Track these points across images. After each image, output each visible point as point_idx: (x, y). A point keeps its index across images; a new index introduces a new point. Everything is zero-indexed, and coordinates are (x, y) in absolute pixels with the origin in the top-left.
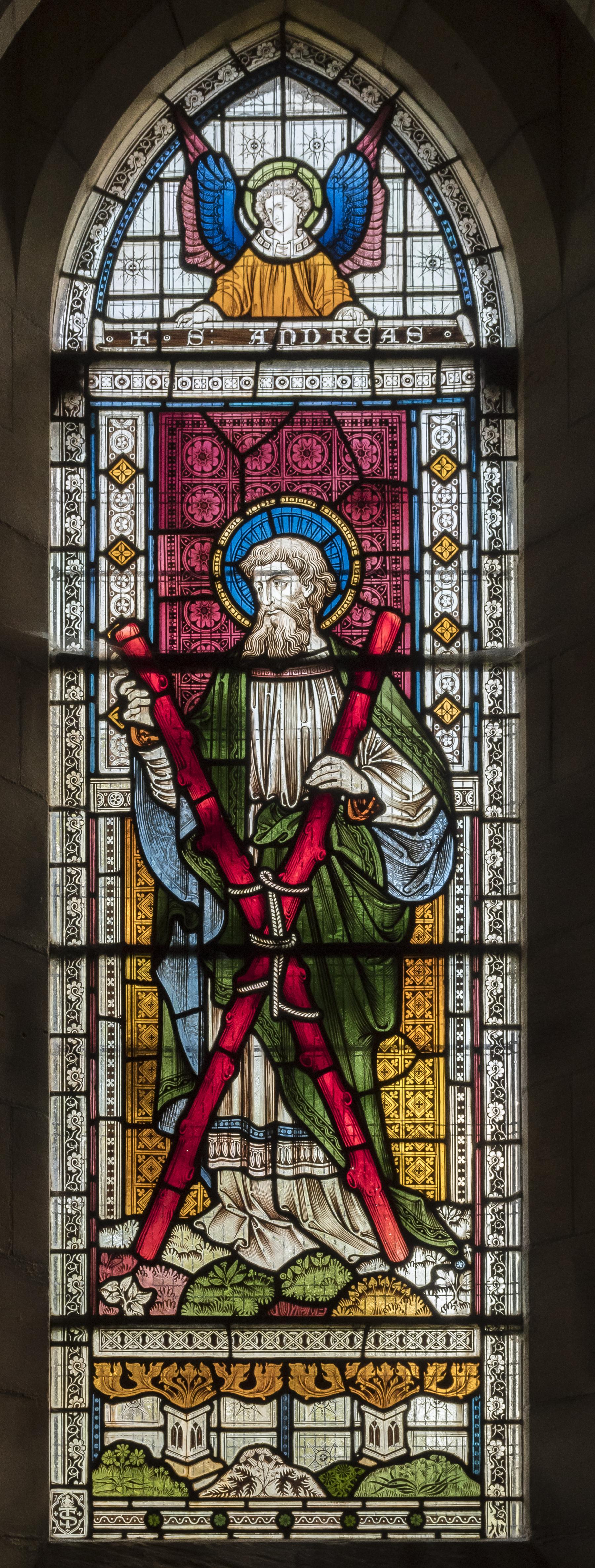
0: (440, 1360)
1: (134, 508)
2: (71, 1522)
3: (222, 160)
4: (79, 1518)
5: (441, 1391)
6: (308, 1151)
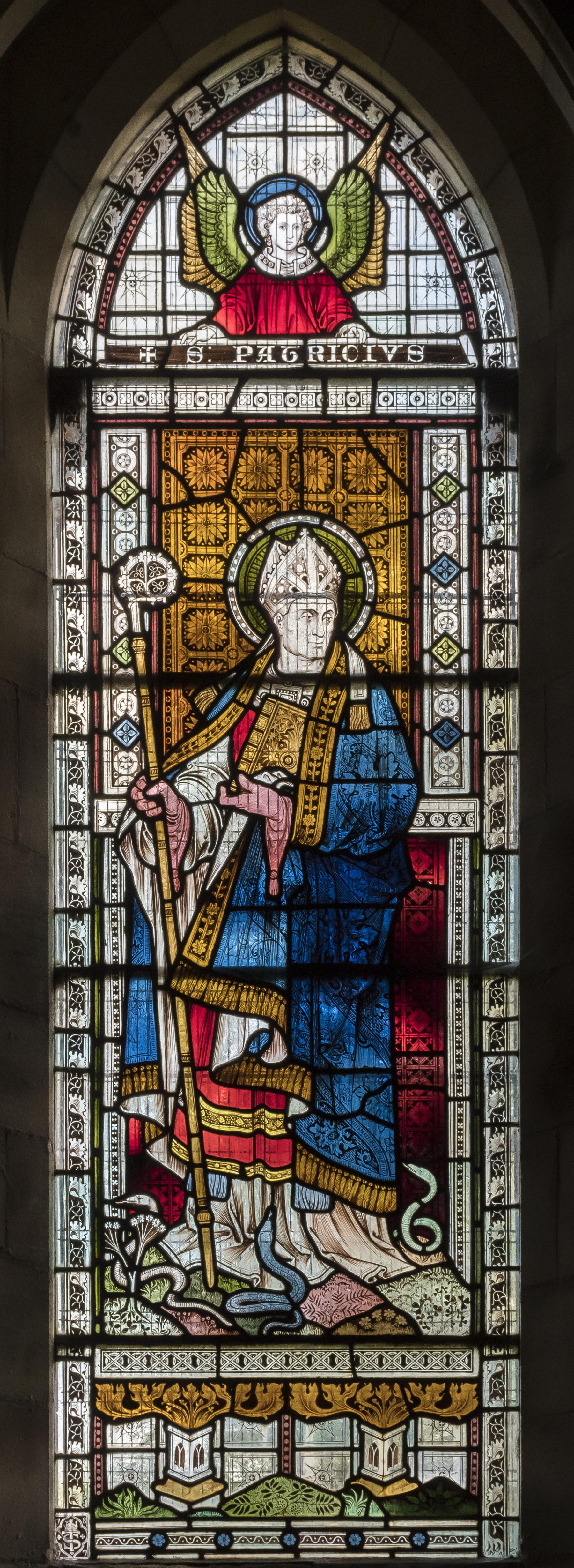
0: (439, 1381)
1: (138, 527)
2: (75, 1545)
3: (222, 176)
4: (81, 1540)
5: (439, 1411)
6: (308, 1172)
